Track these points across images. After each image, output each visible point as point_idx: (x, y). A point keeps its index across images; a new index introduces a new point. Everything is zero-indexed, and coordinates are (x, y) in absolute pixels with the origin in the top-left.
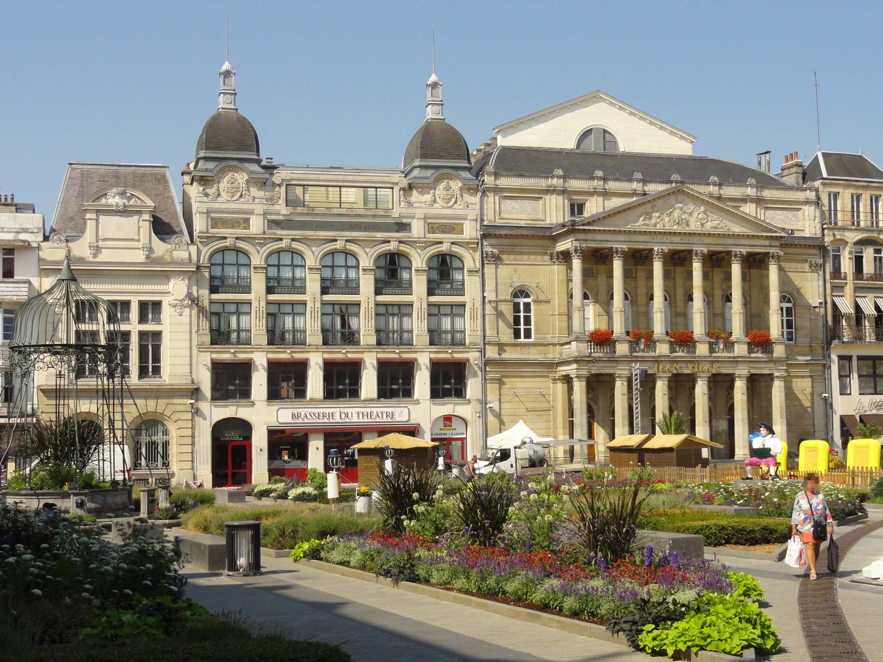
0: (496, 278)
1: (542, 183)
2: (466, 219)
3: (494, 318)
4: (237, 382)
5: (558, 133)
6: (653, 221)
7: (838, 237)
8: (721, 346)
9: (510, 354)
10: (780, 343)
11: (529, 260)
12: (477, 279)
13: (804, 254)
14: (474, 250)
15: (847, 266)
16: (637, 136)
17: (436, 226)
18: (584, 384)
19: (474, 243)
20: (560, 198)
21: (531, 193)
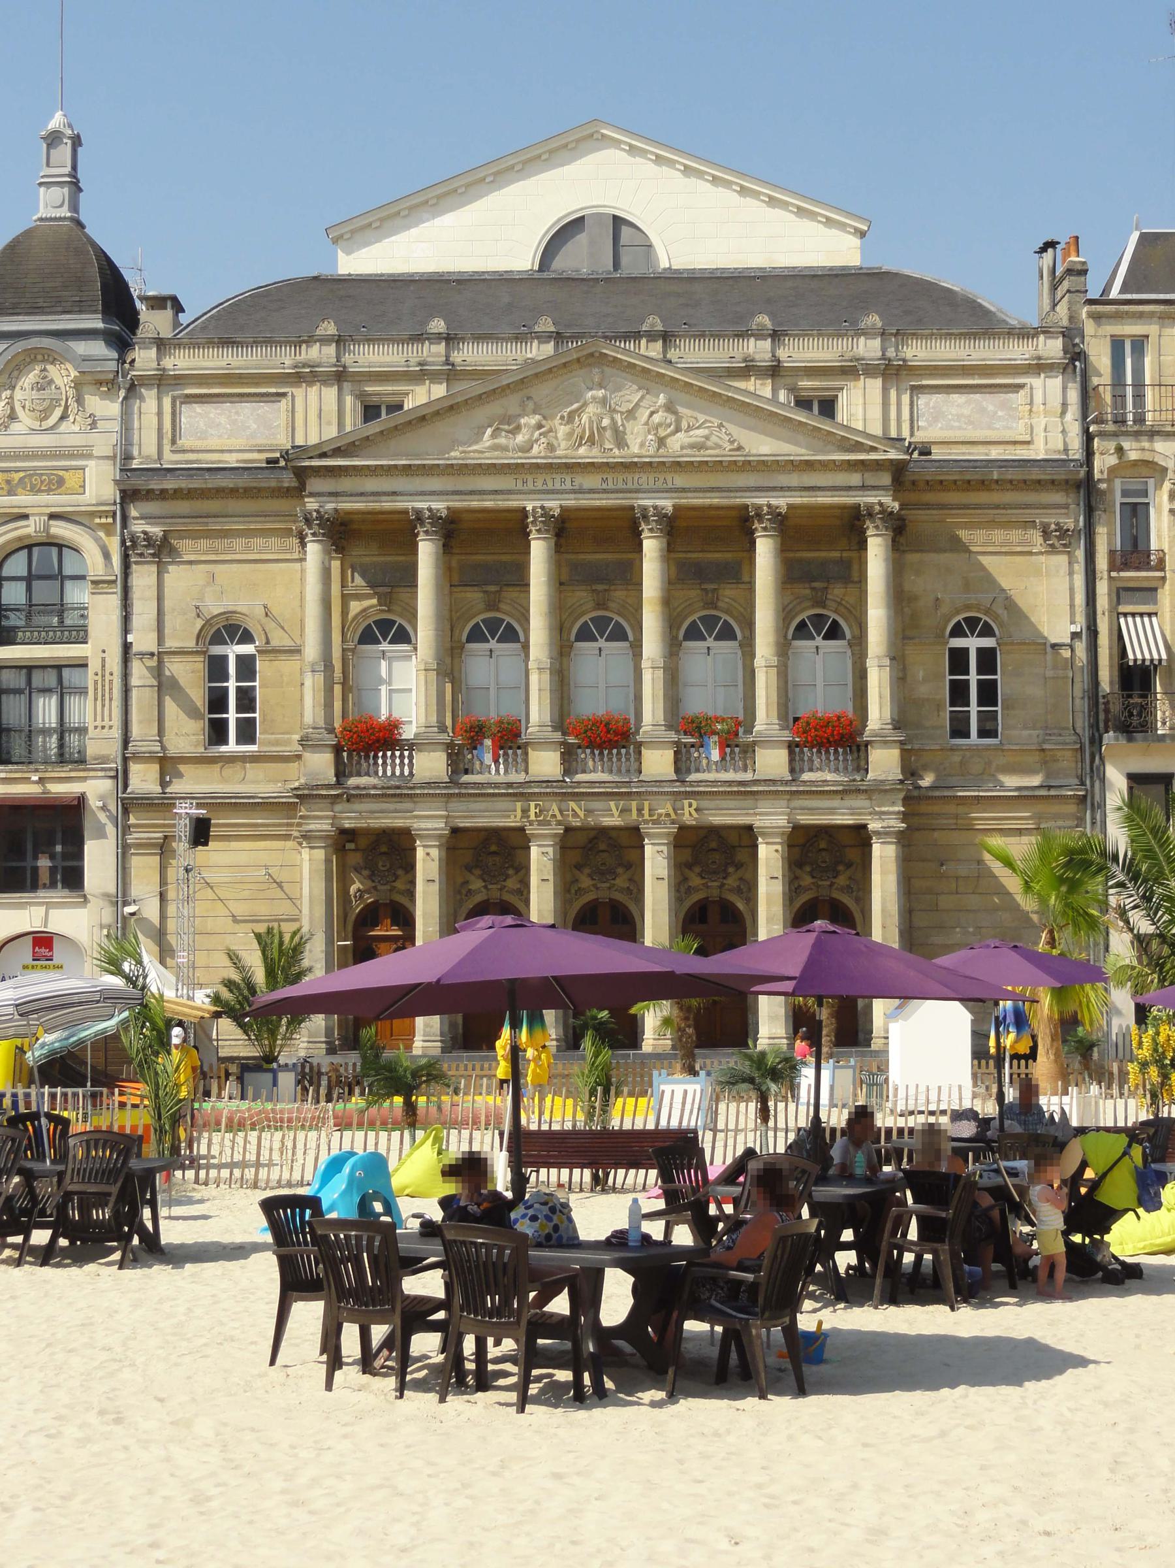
0: (160, 599)
1: (284, 359)
2: (89, 456)
3: (150, 695)
4: (59, 848)
5: (494, 233)
6: (520, 438)
7: (1133, 456)
8: (715, 755)
10: (886, 743)
11: (248, 549)
12: (113, 601)
13: (1028, 506)
16: (702, 225)
17: (17, 476)
18: (320, 854)
19: (100, 514)
20: (331, 393)
21: (257, 385)
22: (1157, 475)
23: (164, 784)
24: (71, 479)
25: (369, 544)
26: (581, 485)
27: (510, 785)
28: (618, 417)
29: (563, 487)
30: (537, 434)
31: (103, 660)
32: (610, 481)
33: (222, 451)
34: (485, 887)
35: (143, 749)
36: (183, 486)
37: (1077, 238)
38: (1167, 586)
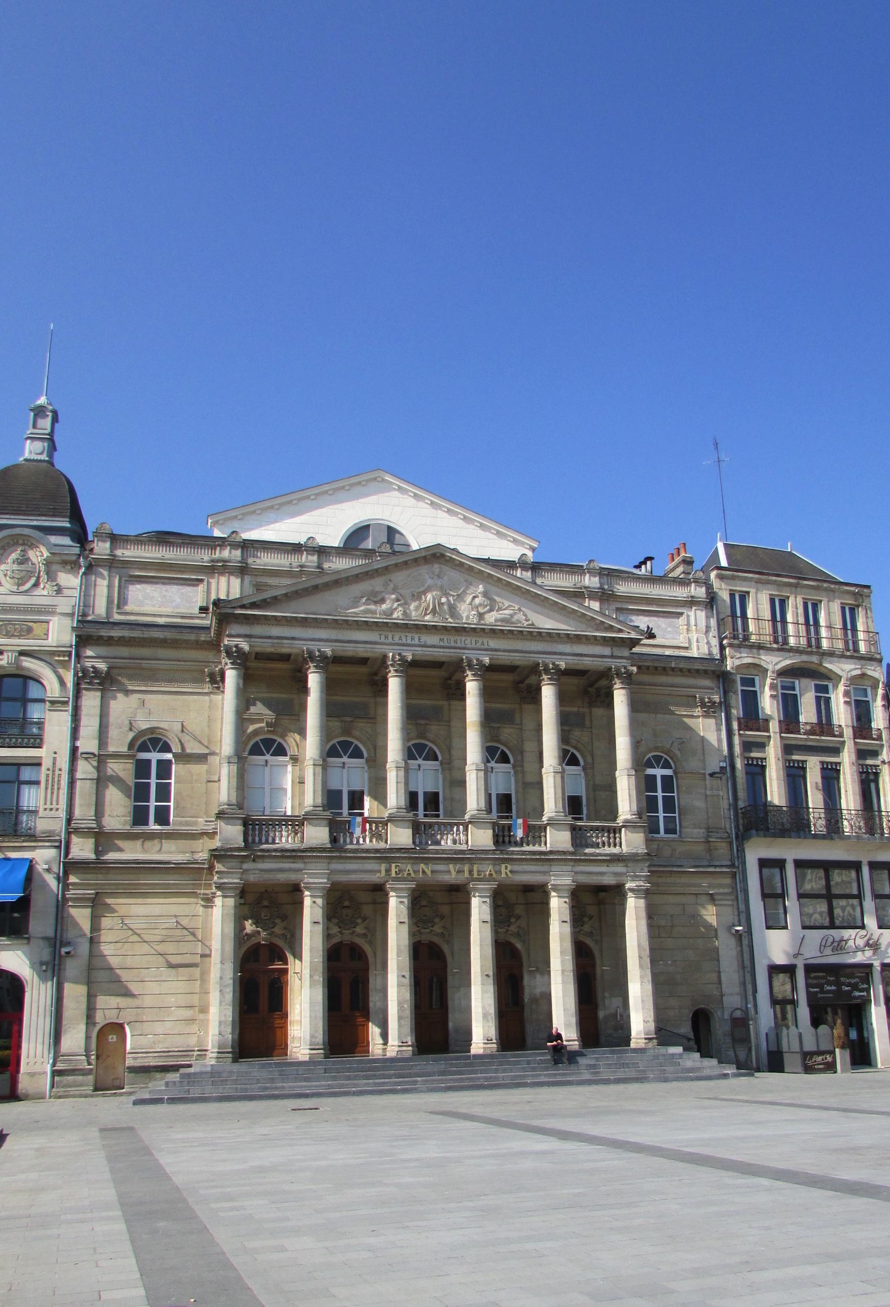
2: (53, 613)
5: (327, 523)
9: (131, 852)
14: (65, 665)
15: (768, 705)
18: (231, 902)
22: (761, 674)
23: (97, 852)
24: (38, 629)
25: (272, 679)
26: (425, 642)
27: (377, 851)
28: (451, 599)
29: (413, 642)
30: (396, 605)
31: (55, 759)
32: (445, 640)
33: (154, 615)
34: (340, 932)
35: (83, 826)
36: (126, 635)
37: (684, 544)
38: (772, 742)
